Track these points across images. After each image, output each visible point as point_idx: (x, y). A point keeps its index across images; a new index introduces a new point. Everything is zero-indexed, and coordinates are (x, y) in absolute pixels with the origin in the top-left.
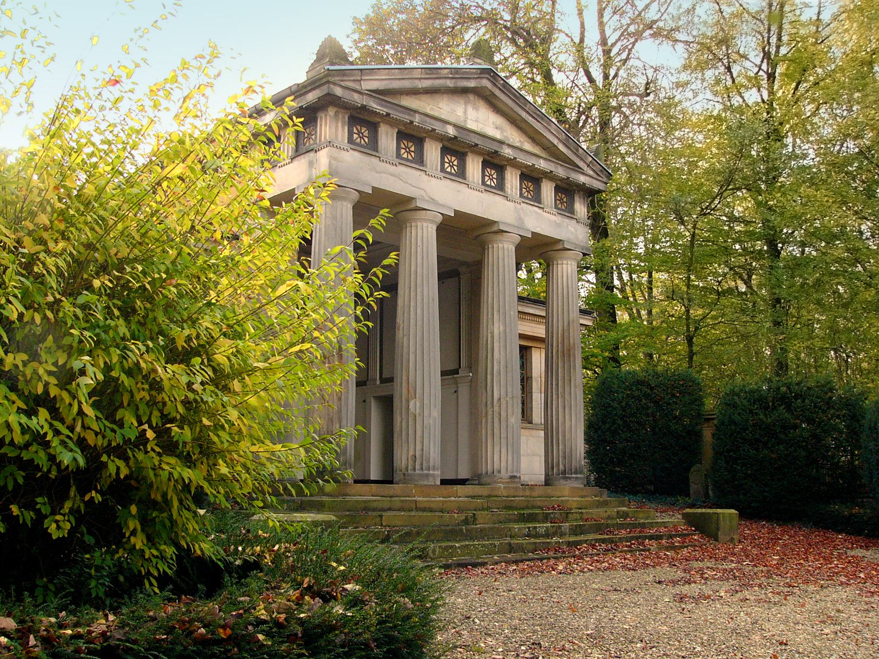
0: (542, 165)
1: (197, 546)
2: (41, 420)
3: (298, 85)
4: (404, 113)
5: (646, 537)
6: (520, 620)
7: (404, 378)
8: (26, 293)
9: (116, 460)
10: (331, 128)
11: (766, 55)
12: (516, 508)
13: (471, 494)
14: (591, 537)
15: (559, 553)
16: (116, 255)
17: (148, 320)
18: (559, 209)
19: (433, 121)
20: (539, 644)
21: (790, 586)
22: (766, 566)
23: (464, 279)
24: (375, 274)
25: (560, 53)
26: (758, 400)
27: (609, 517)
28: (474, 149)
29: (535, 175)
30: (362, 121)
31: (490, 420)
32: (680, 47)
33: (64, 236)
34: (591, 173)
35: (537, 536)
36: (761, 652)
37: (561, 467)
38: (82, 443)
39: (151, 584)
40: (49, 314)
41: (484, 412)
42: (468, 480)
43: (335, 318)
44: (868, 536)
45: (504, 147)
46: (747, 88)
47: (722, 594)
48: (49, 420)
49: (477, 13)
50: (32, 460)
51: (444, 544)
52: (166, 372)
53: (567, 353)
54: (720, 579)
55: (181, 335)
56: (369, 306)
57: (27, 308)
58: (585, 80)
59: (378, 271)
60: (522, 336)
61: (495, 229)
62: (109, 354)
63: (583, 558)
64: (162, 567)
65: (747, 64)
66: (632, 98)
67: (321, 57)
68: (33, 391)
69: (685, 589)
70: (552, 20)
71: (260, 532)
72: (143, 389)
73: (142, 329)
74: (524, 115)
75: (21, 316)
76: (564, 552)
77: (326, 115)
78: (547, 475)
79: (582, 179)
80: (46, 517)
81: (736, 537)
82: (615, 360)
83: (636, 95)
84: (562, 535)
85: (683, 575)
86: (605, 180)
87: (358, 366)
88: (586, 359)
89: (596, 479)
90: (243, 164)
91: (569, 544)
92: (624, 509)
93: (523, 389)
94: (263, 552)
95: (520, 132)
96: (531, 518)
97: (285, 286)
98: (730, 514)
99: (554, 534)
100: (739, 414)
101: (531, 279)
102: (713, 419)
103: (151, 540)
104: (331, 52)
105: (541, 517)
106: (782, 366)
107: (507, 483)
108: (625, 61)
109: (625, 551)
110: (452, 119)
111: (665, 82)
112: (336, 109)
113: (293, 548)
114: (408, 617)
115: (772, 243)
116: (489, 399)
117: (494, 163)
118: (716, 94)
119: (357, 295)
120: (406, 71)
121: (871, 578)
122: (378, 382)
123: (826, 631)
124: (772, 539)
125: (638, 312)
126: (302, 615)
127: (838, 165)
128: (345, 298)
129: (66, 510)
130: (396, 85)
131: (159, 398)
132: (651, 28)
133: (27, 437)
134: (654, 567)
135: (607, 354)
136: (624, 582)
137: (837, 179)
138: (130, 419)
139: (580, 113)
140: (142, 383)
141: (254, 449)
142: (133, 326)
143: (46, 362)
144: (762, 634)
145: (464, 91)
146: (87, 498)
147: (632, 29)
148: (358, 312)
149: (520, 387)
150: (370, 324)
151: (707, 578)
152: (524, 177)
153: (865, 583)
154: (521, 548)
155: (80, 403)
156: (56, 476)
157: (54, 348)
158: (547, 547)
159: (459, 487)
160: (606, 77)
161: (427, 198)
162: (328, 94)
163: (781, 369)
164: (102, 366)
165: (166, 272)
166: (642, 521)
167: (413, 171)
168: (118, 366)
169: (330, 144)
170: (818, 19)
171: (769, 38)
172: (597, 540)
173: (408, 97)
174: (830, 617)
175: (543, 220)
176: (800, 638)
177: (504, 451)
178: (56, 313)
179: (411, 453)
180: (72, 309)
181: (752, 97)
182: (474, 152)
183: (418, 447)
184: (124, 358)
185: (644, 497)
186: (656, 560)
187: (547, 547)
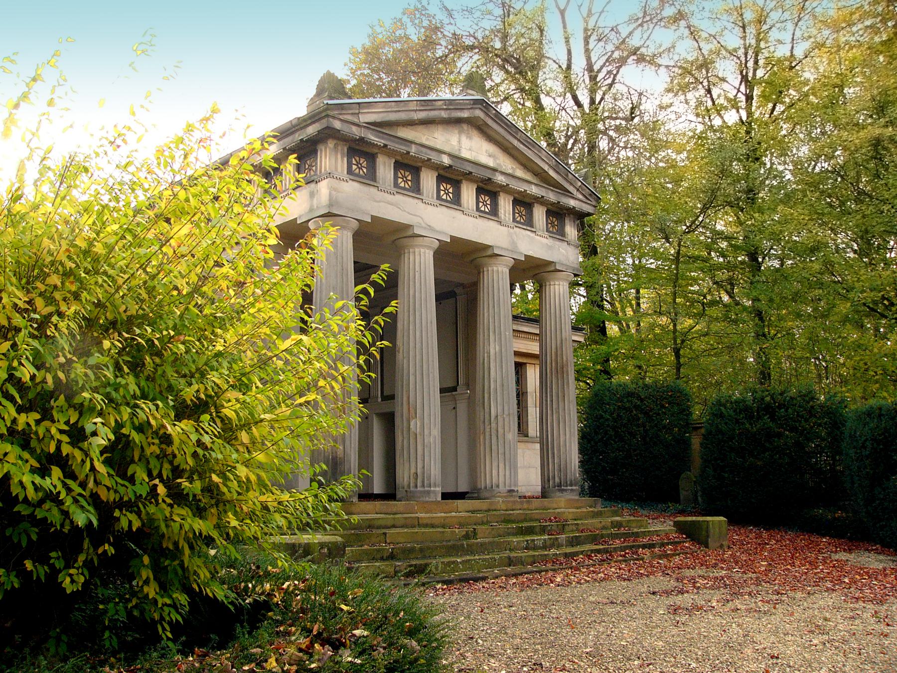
0: (534, 190)
1: (208, 590)
2: (54, 480)
3: (299, 118)
4: (401, 144)
5: (639, 546)
6: (521, 639)
7: (405, 398)
8: (36, 354)
9: (128, 513)
10: (330, 159)
11: (744, 78)
12: (513, 522)
13: (471, 509)
14: (587, 547)
15: (557, 564)
16: (125, 311)
17: (157, 376)
18: (550, 232)
19: (429, 152)
20: (541, 664)
21: (778, 593)
22: (755, 572)
23: (461, 300)
24: (377, 322)
25: (550, 80)
26: (742, 409)
27: (604, 528)
28: (468, 176)
29: (527, 200)
30: (361, 153)
31: (487, 437)
32: (663, 70)
33: (76, 296)
34: (581, 197)
35: (535, 548)
36: (753, 667)
37: (557, 480)
38: (95, 499)
39: (164, 629)
40: (61, 375)
41: (482, 429)
42: (467, 493)
43: (339, 366)
44: (850, 539)
45: (497, 174)
46: (726, 108)
47: (714, 604)
48: (62, 477)
49: (469, 42)
50: (46, 519)
51: (446, 560)
52: (176, 430)
53: (561, 371)
54: (712, 588)
55: (189, 393)
56: (371, 355)
57: (38, 368)
58: (572, 103)
59: (379, 318)
60: (517, 354)
61: (489, 253)
62: (120, 413)
63: (580, 570)
64: (175, 616)
65: (725, 86)
66: (618, 122)
67: (320, 91)
68: (46, 450)
69: (679, 600)
70: (540, 48)
71: (270, 568)
72: (153, 444)
73: (151, 385)
74: (515, 143)
75: (33, 378)
76: (561, 564)
77: (326, 148)
78: (543, 488)
79: (572, 203)
80: (60, 571)
81: (725, 543)
82: (607, 372)
83: (621, 119)
84: (559, 546)
85: (676, 584)
86: (594, 203)
87: (361, 411)
88: (578, 372)
89: (589, 487)
90: (247, 221)
91: (566, 555)
92: (618, 518)
93: (518, 404)
94: (273, 590)
95: (512, 160)
96: (530, 531)
97: (289, 340)
98: (720, 521)
99: (552, 546)
100: (726, 423)
101: (523, 298)
102: (701, 428)
103: (164, 588)
104: (330, 86)
105: (537, 530)
106: (765, 375)
107: (505, 497)
108: (610, 86)
109: (620, 561)
110: (447, 149)
111: (648, 106)
112: (335, 142)
113: (302, 586)
114: (416, 660)
115: (753, 256)
116: (487, 416)
117: (488, 190)
118: (697, 115)
119: (359, 343)
120: (402, 104)
121: (855, 582)
122: (380, 400)
123: (815, 641)
124: (759, 544)
125: (628, 326)
126: (313, 666)
127: (814, 183)
128: (348, 346)
129: (80, 562)
130: (393, 117)
131: (169, 450)
132: (635, 54)
133: (40, 494)
134: (647, 576)
135: (599, 367)
136: (620, 593)
137: (812, 197)
138: (141, 475)
139: (568, 137)
140: (153, 438)
141: (263, 498)
142: (143, 383)
143: (58, 421)
144: (753, 648)
145: (458, 122)
146: (100, 551)
147: (616, 55)
148: (361, 362)
149: (516, 402)
150: (373, 375)
151: (699, 587)
152: (517, 202)
153: (850, 588)
154: (520, 561)
155: (92, 460)
156: (69, 530)
157: (66, 406)
158: (545, 559)
159: (459, 503)
160: (592, 101)
161: (424, 225)
162: (328, 128)
163: (764, 378)
164: (113, 424)
165: (175, 328)
166: (635, 530)
167: (411, 200)
168: (128, 424)
169: (329, 175)
170: (792, 55)
171: (746, 62)
172: (592, 551)
173: (404, 129)
174: (818, 626)
175: (535, 243)
176: (790, 650)
177: (502, 465)
178: (67, 373)
179: (413, 471)
180: (83, 370)
181: (731, 117)
182: (467, 180)
183: (420, 466)
184: (134, 415)
185: (636, 504)
186: (649, 569)
187: (545, 559)
